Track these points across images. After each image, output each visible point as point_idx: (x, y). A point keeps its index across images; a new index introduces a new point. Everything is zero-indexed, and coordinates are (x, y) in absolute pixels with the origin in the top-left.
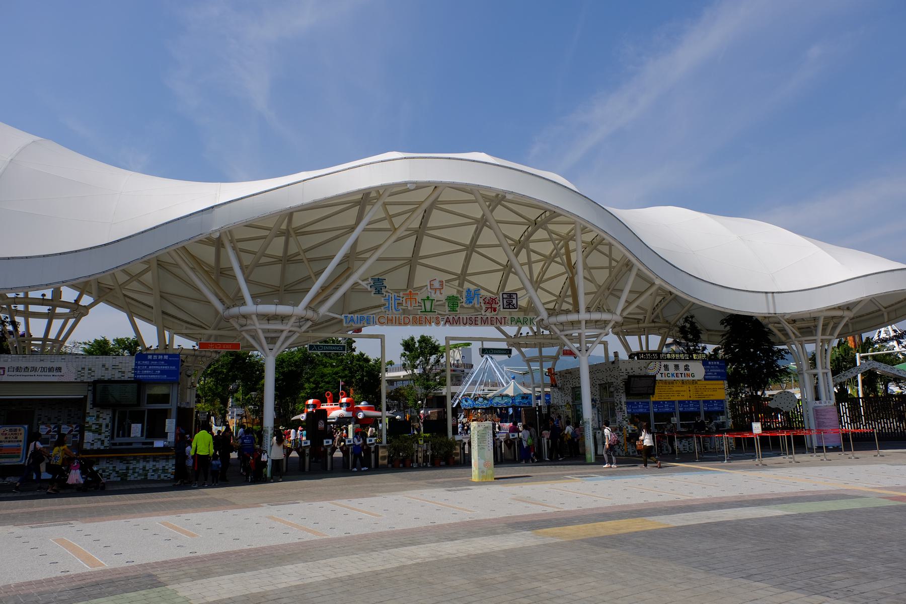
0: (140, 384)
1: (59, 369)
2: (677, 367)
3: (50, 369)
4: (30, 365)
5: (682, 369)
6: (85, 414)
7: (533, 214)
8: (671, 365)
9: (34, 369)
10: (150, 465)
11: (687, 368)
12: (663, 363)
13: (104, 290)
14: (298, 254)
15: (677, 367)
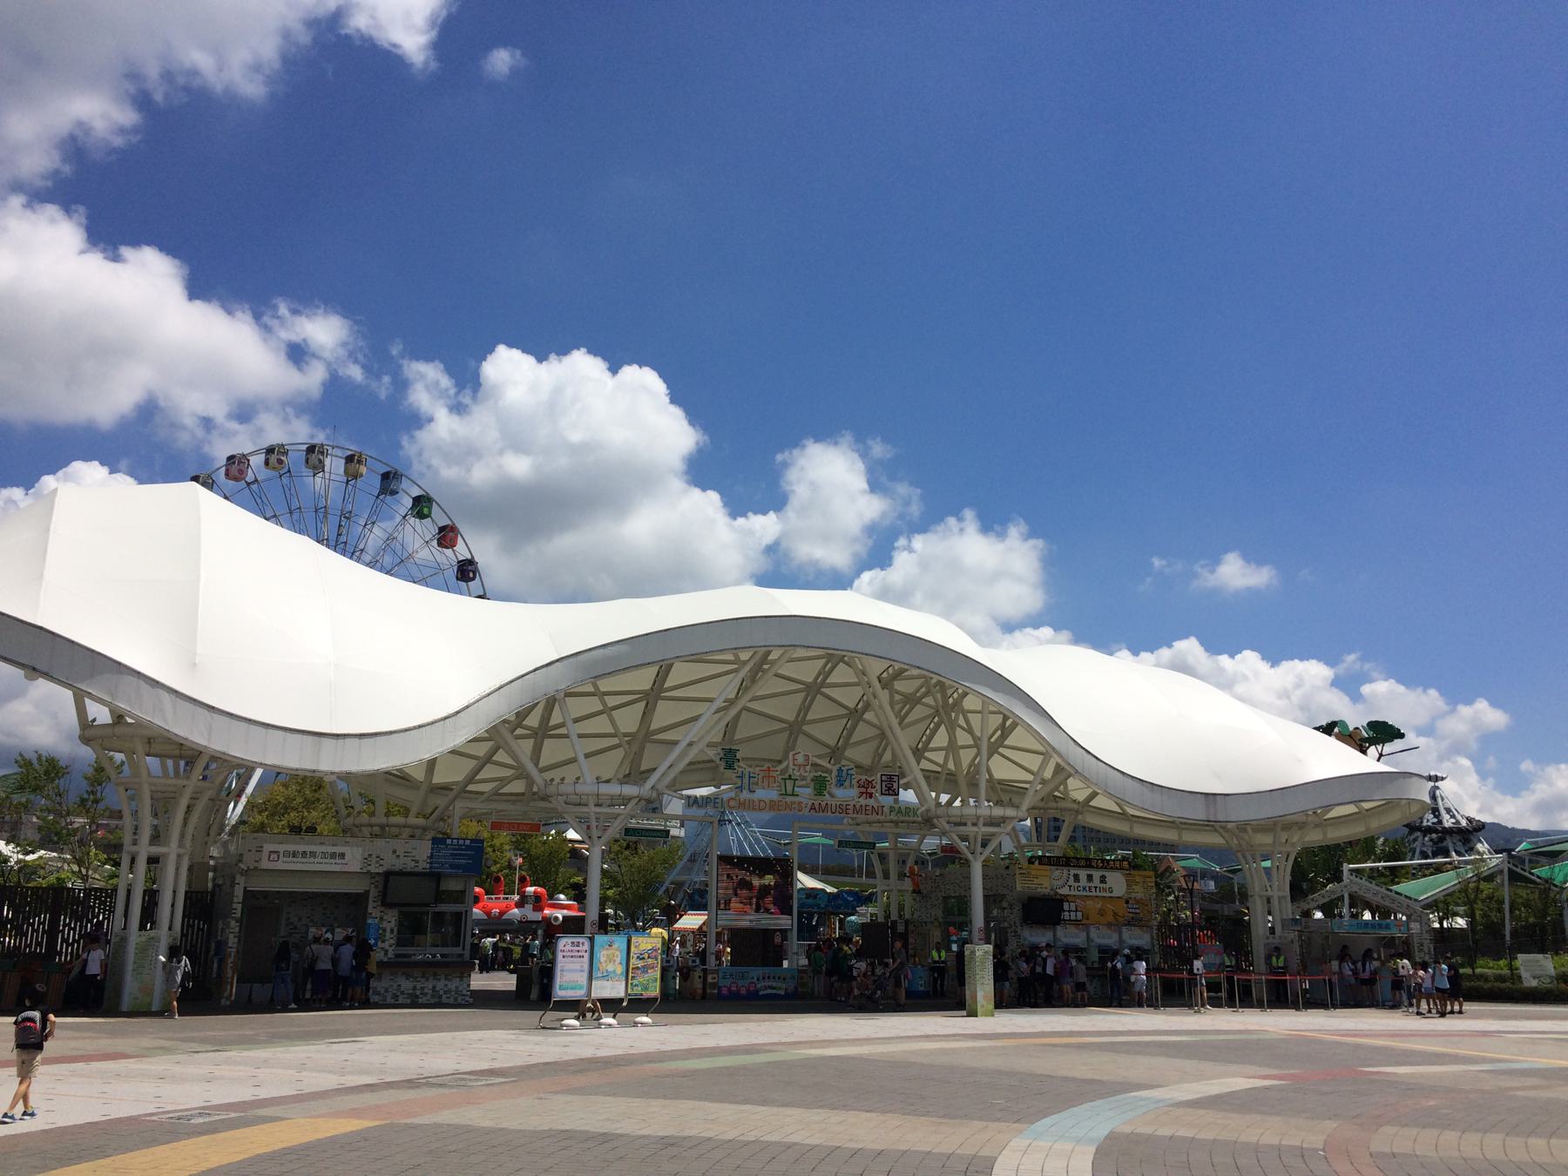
0: (435, 876)
1: (342, 855)
2: (1090, 878)
3: (333, 856)
4: (308, 848)
5: (1096, 882)
6: (365, 915)
7: (643, 680)
8: (1083, 874)
9: (313, 854)
10: (440, 985)
11: (1103, 880)
12: (1073, 872)
13: (1111, 796)
14: (562, 725)
15: (1090, 878)
